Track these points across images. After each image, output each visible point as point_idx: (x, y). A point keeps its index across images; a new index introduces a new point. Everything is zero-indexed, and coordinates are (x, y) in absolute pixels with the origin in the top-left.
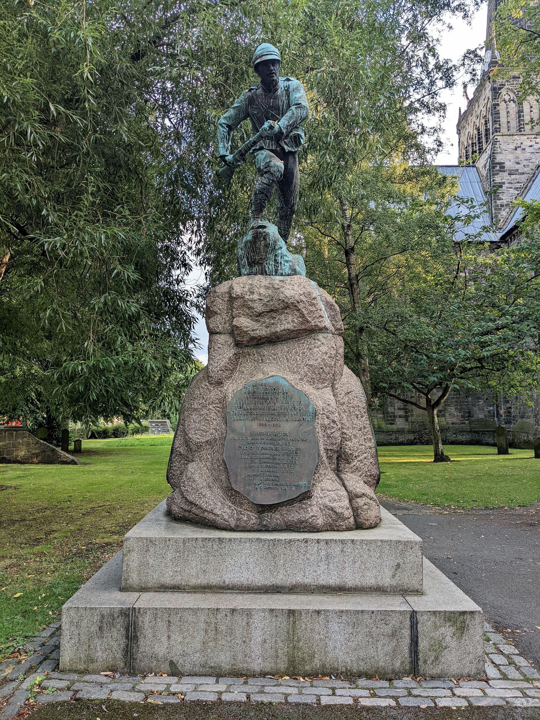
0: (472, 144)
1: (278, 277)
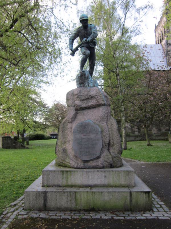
0: (160, 36)
1: (89, 88)
